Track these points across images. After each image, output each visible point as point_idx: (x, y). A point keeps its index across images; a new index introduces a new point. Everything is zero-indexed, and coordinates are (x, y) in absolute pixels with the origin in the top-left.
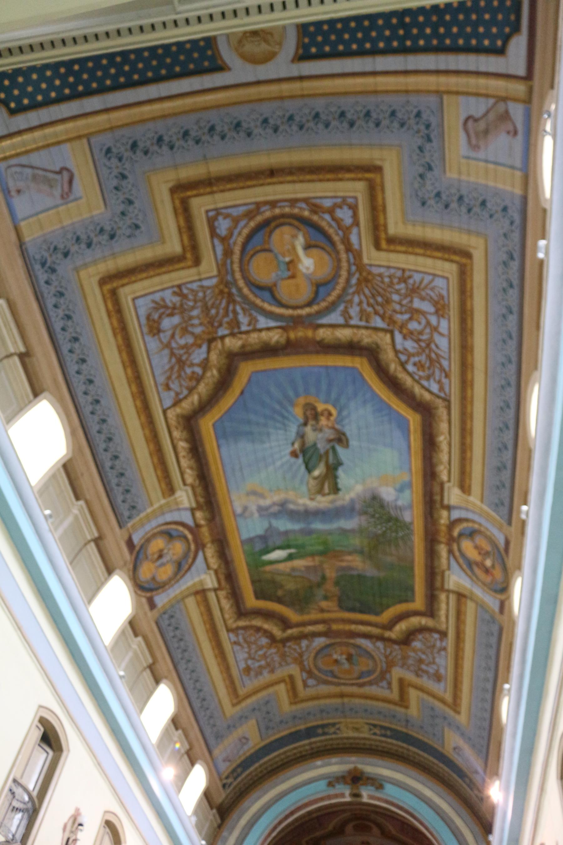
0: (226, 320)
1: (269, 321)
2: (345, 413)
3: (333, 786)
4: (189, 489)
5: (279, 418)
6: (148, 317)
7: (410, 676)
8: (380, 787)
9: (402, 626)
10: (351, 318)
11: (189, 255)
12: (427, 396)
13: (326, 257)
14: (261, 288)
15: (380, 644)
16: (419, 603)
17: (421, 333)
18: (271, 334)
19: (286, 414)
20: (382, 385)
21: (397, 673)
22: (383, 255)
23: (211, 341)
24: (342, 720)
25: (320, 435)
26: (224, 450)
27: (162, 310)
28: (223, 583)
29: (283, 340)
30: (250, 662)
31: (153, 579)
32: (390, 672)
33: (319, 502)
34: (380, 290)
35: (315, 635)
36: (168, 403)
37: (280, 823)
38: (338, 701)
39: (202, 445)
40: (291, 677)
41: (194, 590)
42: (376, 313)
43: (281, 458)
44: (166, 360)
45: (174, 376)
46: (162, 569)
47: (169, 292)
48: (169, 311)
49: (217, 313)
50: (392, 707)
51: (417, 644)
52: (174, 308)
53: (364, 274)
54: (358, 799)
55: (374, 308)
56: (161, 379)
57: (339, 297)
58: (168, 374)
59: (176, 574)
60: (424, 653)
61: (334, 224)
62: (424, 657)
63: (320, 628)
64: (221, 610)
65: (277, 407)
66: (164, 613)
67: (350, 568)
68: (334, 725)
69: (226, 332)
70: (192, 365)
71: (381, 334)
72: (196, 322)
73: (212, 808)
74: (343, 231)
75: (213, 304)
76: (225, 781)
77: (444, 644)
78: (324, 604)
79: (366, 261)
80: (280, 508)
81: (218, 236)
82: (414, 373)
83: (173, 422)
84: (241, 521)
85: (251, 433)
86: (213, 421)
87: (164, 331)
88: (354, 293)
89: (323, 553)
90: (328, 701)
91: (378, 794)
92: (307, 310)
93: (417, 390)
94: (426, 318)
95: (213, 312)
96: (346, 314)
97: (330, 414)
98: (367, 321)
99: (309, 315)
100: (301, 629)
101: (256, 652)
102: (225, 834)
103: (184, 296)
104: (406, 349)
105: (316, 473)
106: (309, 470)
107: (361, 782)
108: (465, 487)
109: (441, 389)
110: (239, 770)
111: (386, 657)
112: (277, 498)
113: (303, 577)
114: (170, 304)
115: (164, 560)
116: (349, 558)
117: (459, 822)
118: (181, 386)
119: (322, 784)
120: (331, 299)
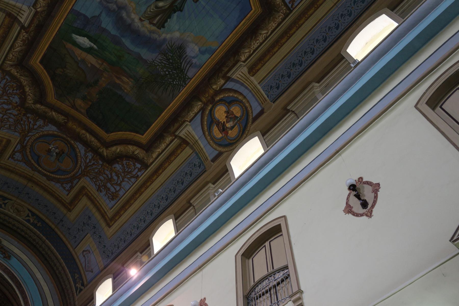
7: (92, 188)
8: (9, 258)
9: (118, 149)
15: (90, 155)
16: (144, 138)
21: (85, 182)
32: (80, 179)
35: (53, 121)
51: (118, 167)
62: (115, 178)
63: (60, 118)
64: (12, 47)
77: (139, 174)
78: (79, 102)
80: (117, 9)
108: (253, 70)
116: (125, 79)
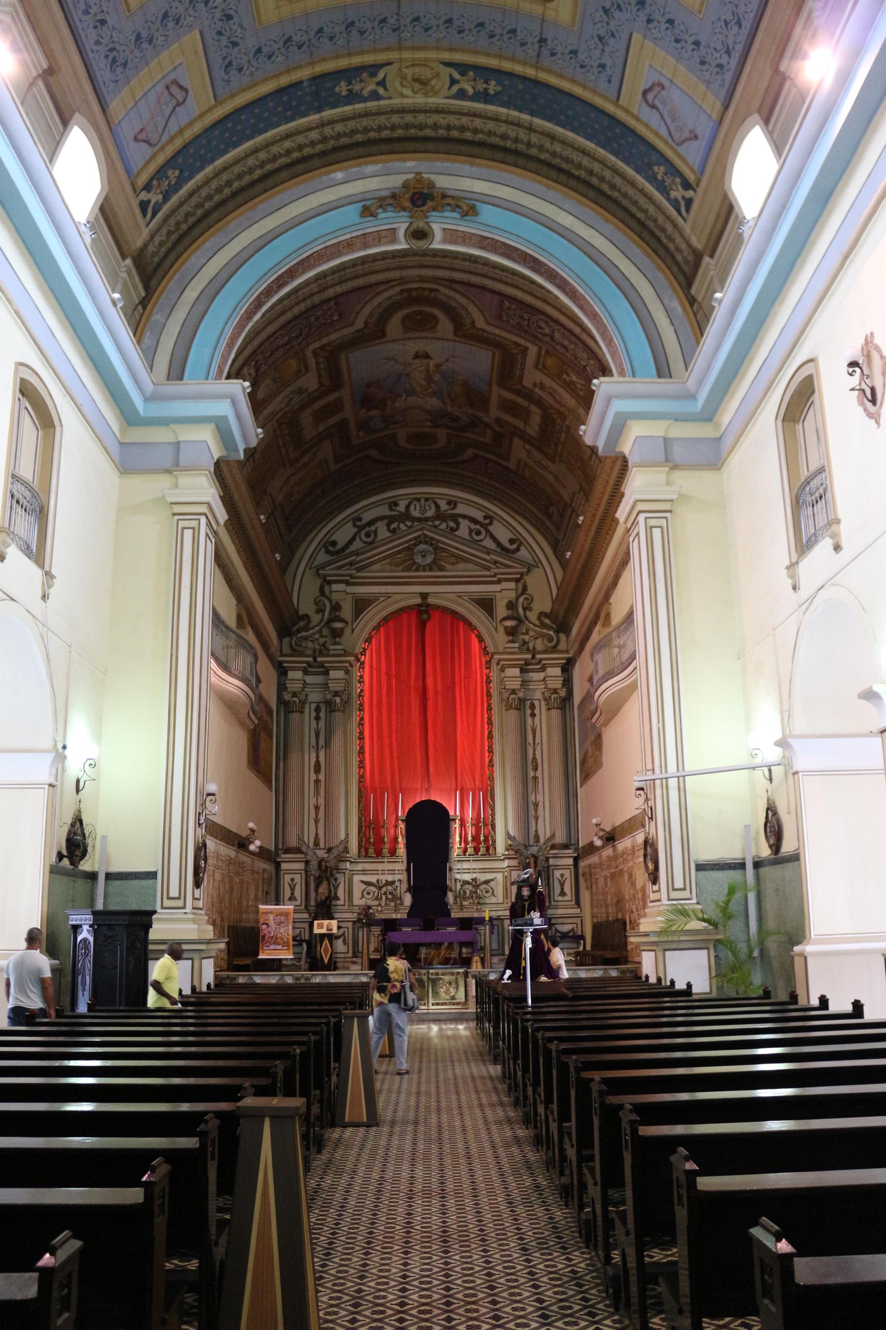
3: (374, 215)
24: (393, 56)
37: (268, 292)
54: (422, 244)
73: (124, 257)
76: (144, 196)
91: (465, 227)
102: (157, 317)
107: (430, 204)
110: (173, 174)
117: (625, 266)
119: (352, 213)
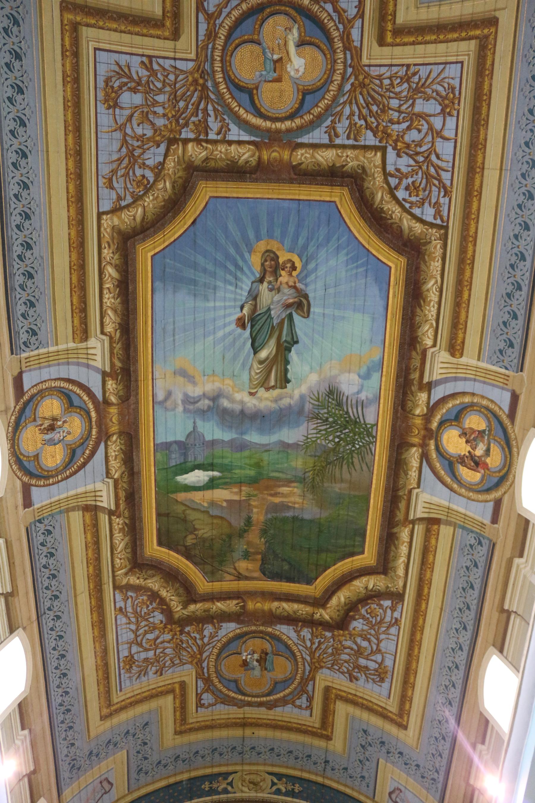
0: (193, 119)
1: (242, 133)
2: (311, 266)
4: (106, 339)
5: (232, 268)
6: (107, 81)
10: (337, 136)
11: (168, 23)
12: (418, 228)
13: (320, 57)
14: (240, 88)
15: (306, 633)
17: (419, 144)
18: (241, 150)
19: (241, 263)
20: (362, 223)
22: (386, 50)
23: (172, 142)
24: (238, 768)
25: (277, 298)
26: (158, 296)
27: (125, 80)
28: (122, 506)
29: (253, 161)
30: (135, 649)
31: (37, 457)
32: (314, 679)
33: (261, 400)
34: (376, 96)
36: (106, 206)
38: (238, 732)
39: (134, 281)
40: (183, 685)
41: (82, 502)
42: (368, 127)
43: (225, 326)
44: (116, 146)
45: (120, 173)
46: (49, 449)
47: (139, 59)
48: (133, 85)
49: (187, 107)
50: (308, 739)
51: (357, 625)
52: (139, 84)
53: (361, 77)
55: (366, 121)
56: (105, 170)
57: (328, 108)
58: (115, 165)
59: (67, 465)
60: (365, 639)
61: (335, 16)
62: (365, 644)
63: (231, 606)
65: (232, 251)
66: (40, 521)
67: (285, 507)
68: (225, 775)
69: (192, 136)
70: (144, 166)
71: (370, 154)
72: (159, 110)
74: (343, 24)
75: (184, 94)
78: (243, 566)
79: (365, 61)
80: (211, 404)
81: (205, 11)
82: (404, 200)
83: (106, 236)
84: (159, 411)
85: (194, 282)
86: (152, 253)
87: (121, 108)
88: (344, 103)
89: (253, 481)
90: (224, 733)
92: (288, 124)
93: (407, 223)
94: (428, 122)
95: (182, 104)
96: (332, 132)
97: (294, 268)
98: (356, 140)
99: (289, 131)
100: (207, 605)
101: (146, 633)
103: (154, 73)
104: (398, 170)
105: (264, 354)
106: (256, 350)
109: (438, 213)
111: (312, 654)
112: (210, 387)
113: (221, 518)
114: (135, 77)
115: (56, 436)
116: (285, 490)
118: (126, 188)
120: (317, 111)
